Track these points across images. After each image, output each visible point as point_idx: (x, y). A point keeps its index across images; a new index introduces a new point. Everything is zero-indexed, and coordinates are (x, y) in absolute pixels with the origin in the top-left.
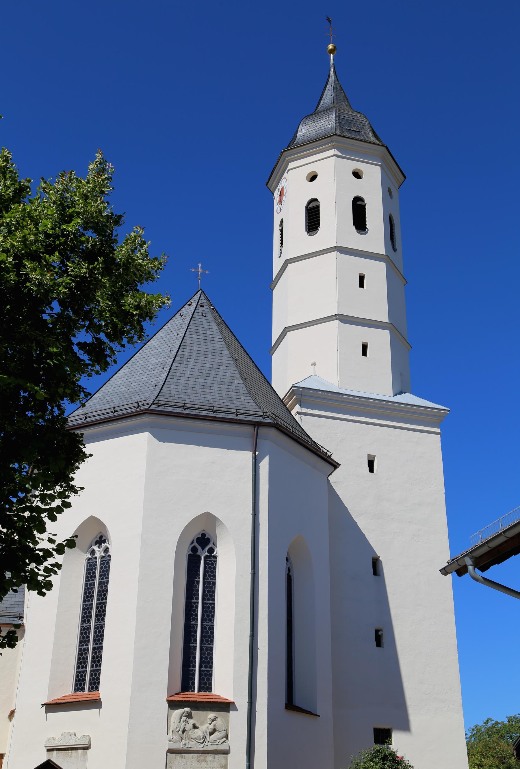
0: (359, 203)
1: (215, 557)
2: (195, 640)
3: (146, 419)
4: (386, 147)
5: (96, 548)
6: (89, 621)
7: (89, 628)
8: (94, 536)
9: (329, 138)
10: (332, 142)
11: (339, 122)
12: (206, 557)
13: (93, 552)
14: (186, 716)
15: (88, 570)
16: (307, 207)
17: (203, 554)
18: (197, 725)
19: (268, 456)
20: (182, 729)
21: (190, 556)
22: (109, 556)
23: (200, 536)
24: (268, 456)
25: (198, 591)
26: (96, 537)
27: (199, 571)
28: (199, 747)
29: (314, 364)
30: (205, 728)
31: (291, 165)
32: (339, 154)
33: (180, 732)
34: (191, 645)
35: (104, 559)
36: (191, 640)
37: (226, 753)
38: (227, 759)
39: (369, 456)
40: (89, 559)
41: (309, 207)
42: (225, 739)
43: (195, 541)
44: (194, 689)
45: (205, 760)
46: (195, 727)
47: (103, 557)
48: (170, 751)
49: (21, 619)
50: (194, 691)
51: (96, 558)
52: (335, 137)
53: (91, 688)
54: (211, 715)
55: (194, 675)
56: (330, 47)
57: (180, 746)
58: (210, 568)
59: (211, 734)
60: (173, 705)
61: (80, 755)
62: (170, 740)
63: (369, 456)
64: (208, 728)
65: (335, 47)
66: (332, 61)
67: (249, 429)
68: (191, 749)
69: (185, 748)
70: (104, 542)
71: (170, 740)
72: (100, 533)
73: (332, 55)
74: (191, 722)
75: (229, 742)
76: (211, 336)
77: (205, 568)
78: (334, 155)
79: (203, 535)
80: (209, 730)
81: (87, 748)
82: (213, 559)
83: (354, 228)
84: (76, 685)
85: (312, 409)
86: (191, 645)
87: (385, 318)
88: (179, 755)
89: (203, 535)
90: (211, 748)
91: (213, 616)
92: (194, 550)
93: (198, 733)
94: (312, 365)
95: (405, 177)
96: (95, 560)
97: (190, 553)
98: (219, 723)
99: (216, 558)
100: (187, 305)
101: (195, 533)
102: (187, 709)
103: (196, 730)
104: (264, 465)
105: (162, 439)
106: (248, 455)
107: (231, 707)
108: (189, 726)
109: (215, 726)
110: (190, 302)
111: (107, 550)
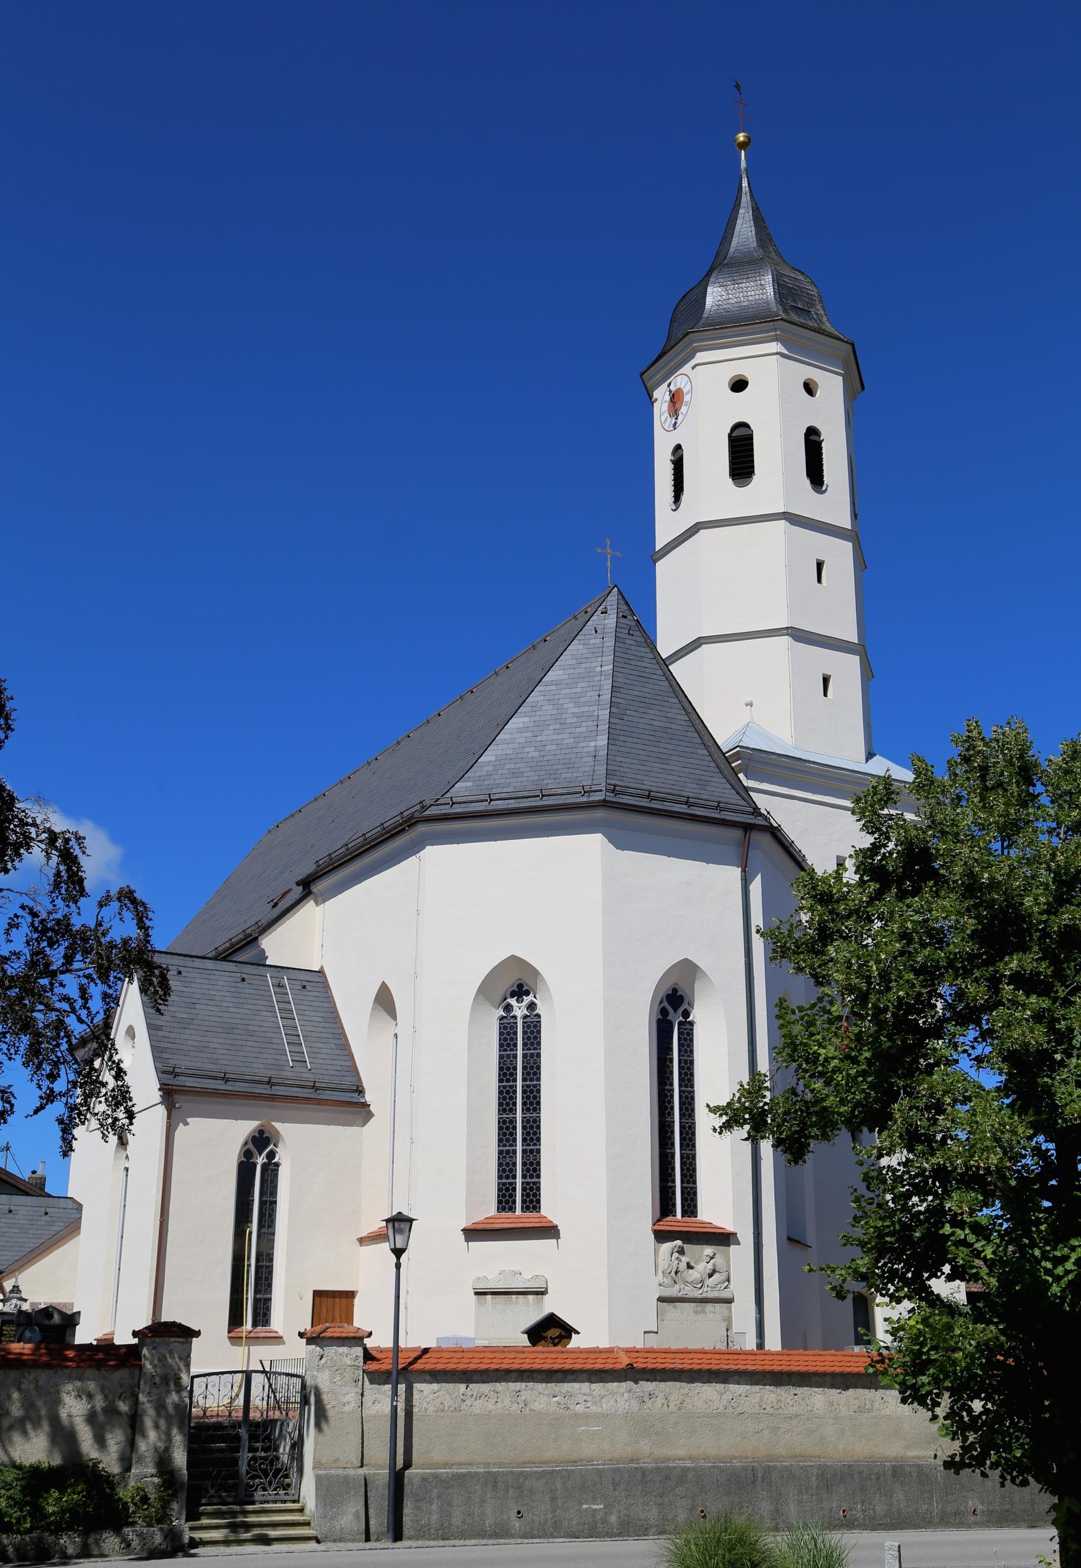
0: (813, 437)
1: (691, 1024)
2: (673, 1144)
3: (600, 814)
4: (853, 345)
5: (513, 1001)
6: (513, 1110)
7: (513, 1121)
8: (511, 982)
9: (772, 323)
10: (775, 330)
11: (779, 292)
12: (680, 1023)
13: (508, 1008)
14: (678, 1252)
15: (501, 1034)
16: (730, 436)
17: (677, 1019)
18: (692, 1264)
19: (759, 876)
20: (674, 1270)
21: (659, 1021)
22: (538, 1016)
23: (670, 992)
24: (759, 876)
25: (672, 1073)
26: (513, 986)
27: (672, 1043)
28: (697, 1294)
29: (750, 704)
30: (702, 1268)
31: (700, 357)
32: (786, 352)
33: (673, 1274)
34: (668, 1151)
35: (528, 1020)
36: (667, 1144)
37: (729, 1301)
38: (730, 1310)
39: (838, 857)
40: (502, 1018)
41: (733, 435)
42: (727, 1283)
43: (665, 1000)
44: (675, 1212)
45: (703, 1311)
46: (689, 1267)
47: (525, 1017)
48: (661, 1299)
49: (361, 1095)
50: (675, 1216)
51: (515, 1017)
52: (781, 322)
53: (526, 1208)
54: (708, 1250)
55: (674, 1193)
56: (741, 137)
57: (673, 1292)
58: (685, 1039)
59: (710, 1276)
60: (661, 1236)
61: (531, 1302)
62: (660, 1285)
63: (838, 857)
64: (706, 1267)
65: (749, 138)
66: (743, 164)
67: (737, 833)
68: (687, 1296)
69: (680, 1295)
70: (527, 993)
71: (660, 1285)
72: (520, 979)
73: (743, 152)
74: (685, 1259)
75: (731, 1286)
76: (648, 670)
77: (679, 1039)
78: (777, 353)
79: (675, 990)
80: (708, 1271)
81: (543, 1293)
82: (688, 1026)
83: (808, 482)
84: (500, 1202)
85: (762, 781)
86: (668, 1151)
87: (852, 637)
88: (672, 1304)
89: (675, 990)
90: (711, 1295)
91: (693, 1110)
92: (664, 1012)
93: (694, 1275)
94: (747, 705)
95: (863, 388)
96: (512, 1021)
97: (660, 1017)
98: (719, 1260)
99: (693, 1025)
100: (598, 612)
101: (666, 989)
102: (679, 1243)
103: (691, 1271)
104: (756, 887)
105: (620, 845)
106: (736, 872)
107: (731, 1238)
108: (683, 1266)
109: (714, 1265)
110: (602, 607)
111: (532, 1006)
